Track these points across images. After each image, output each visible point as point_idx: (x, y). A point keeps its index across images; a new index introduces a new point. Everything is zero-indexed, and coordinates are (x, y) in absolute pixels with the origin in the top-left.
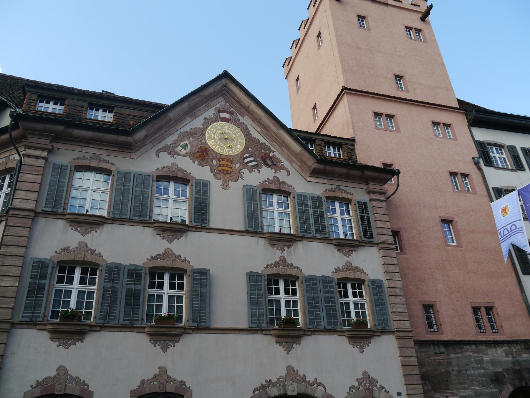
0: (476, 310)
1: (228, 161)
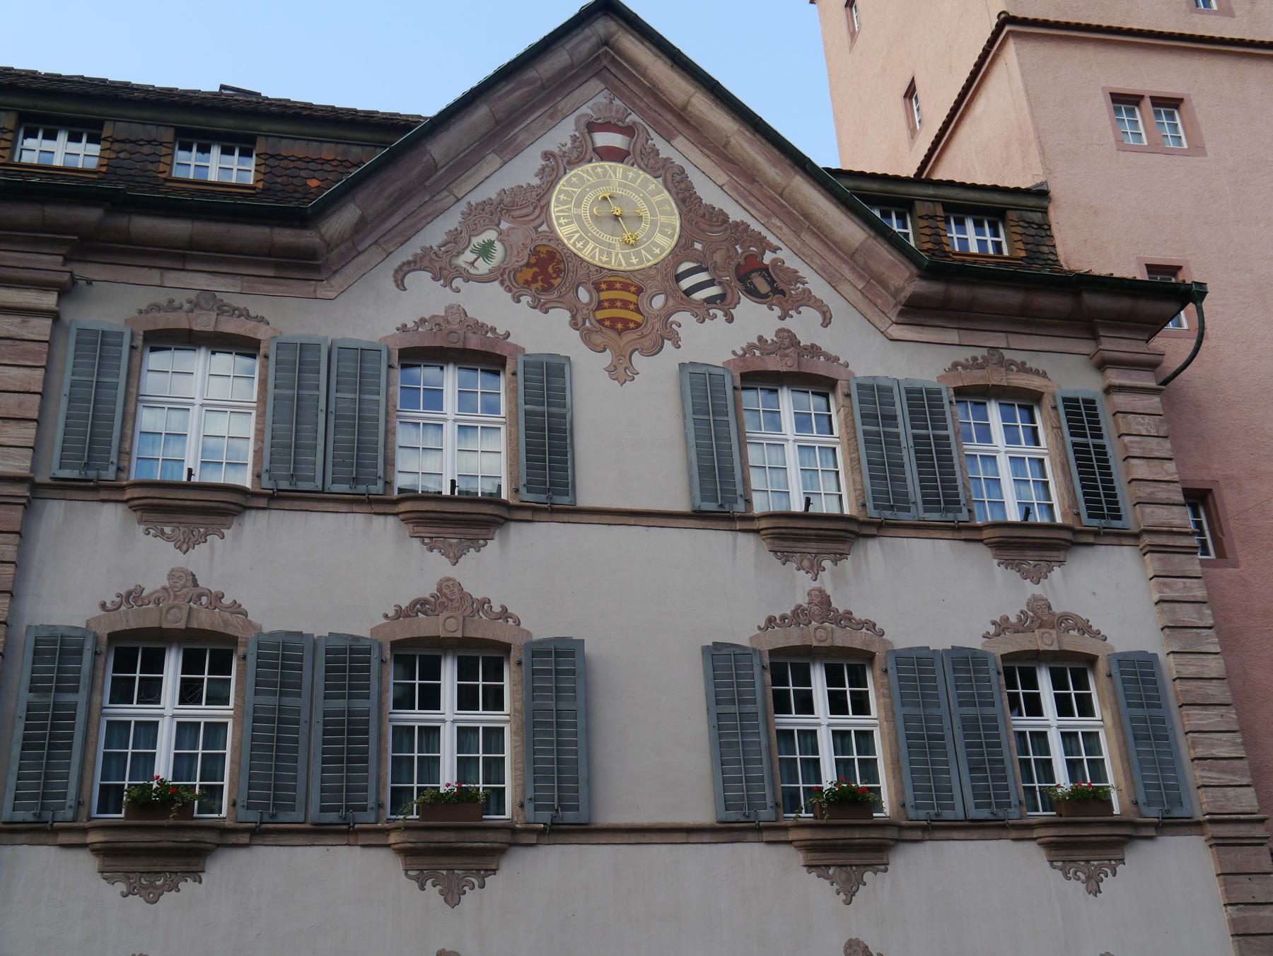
1: (625, 287)
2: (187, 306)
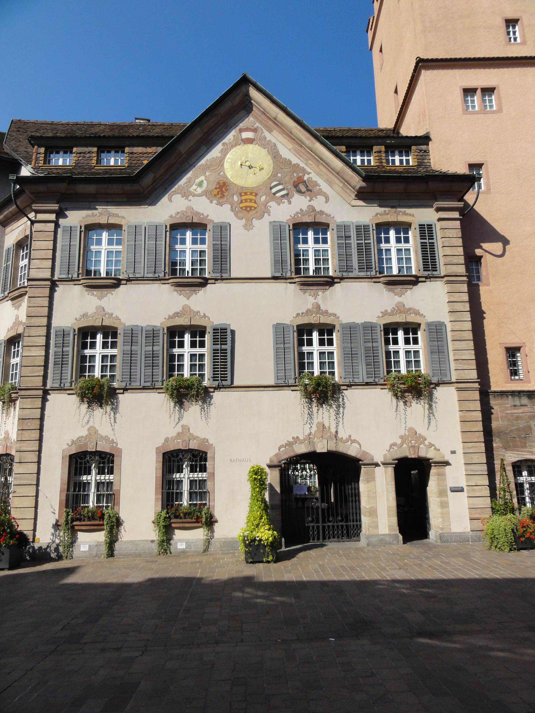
1: (251, 194)
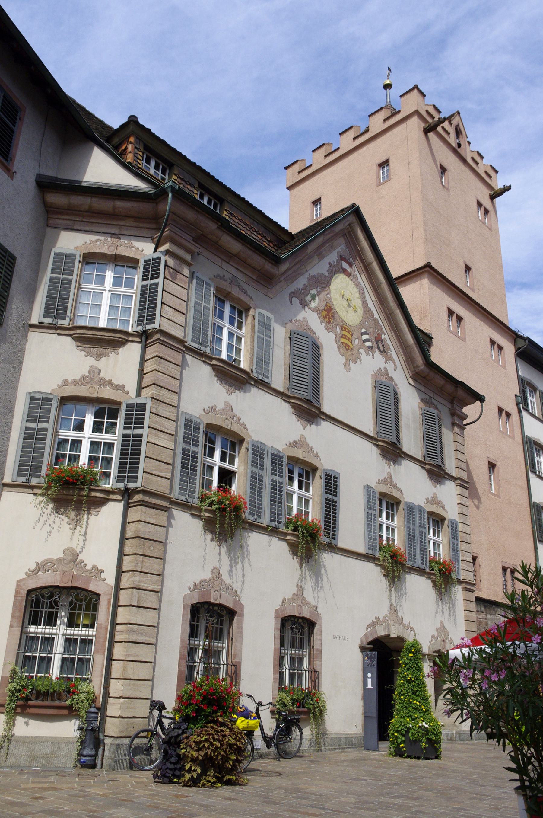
0: (505, 569)
1: (349, 332)
2: (229, 281)
